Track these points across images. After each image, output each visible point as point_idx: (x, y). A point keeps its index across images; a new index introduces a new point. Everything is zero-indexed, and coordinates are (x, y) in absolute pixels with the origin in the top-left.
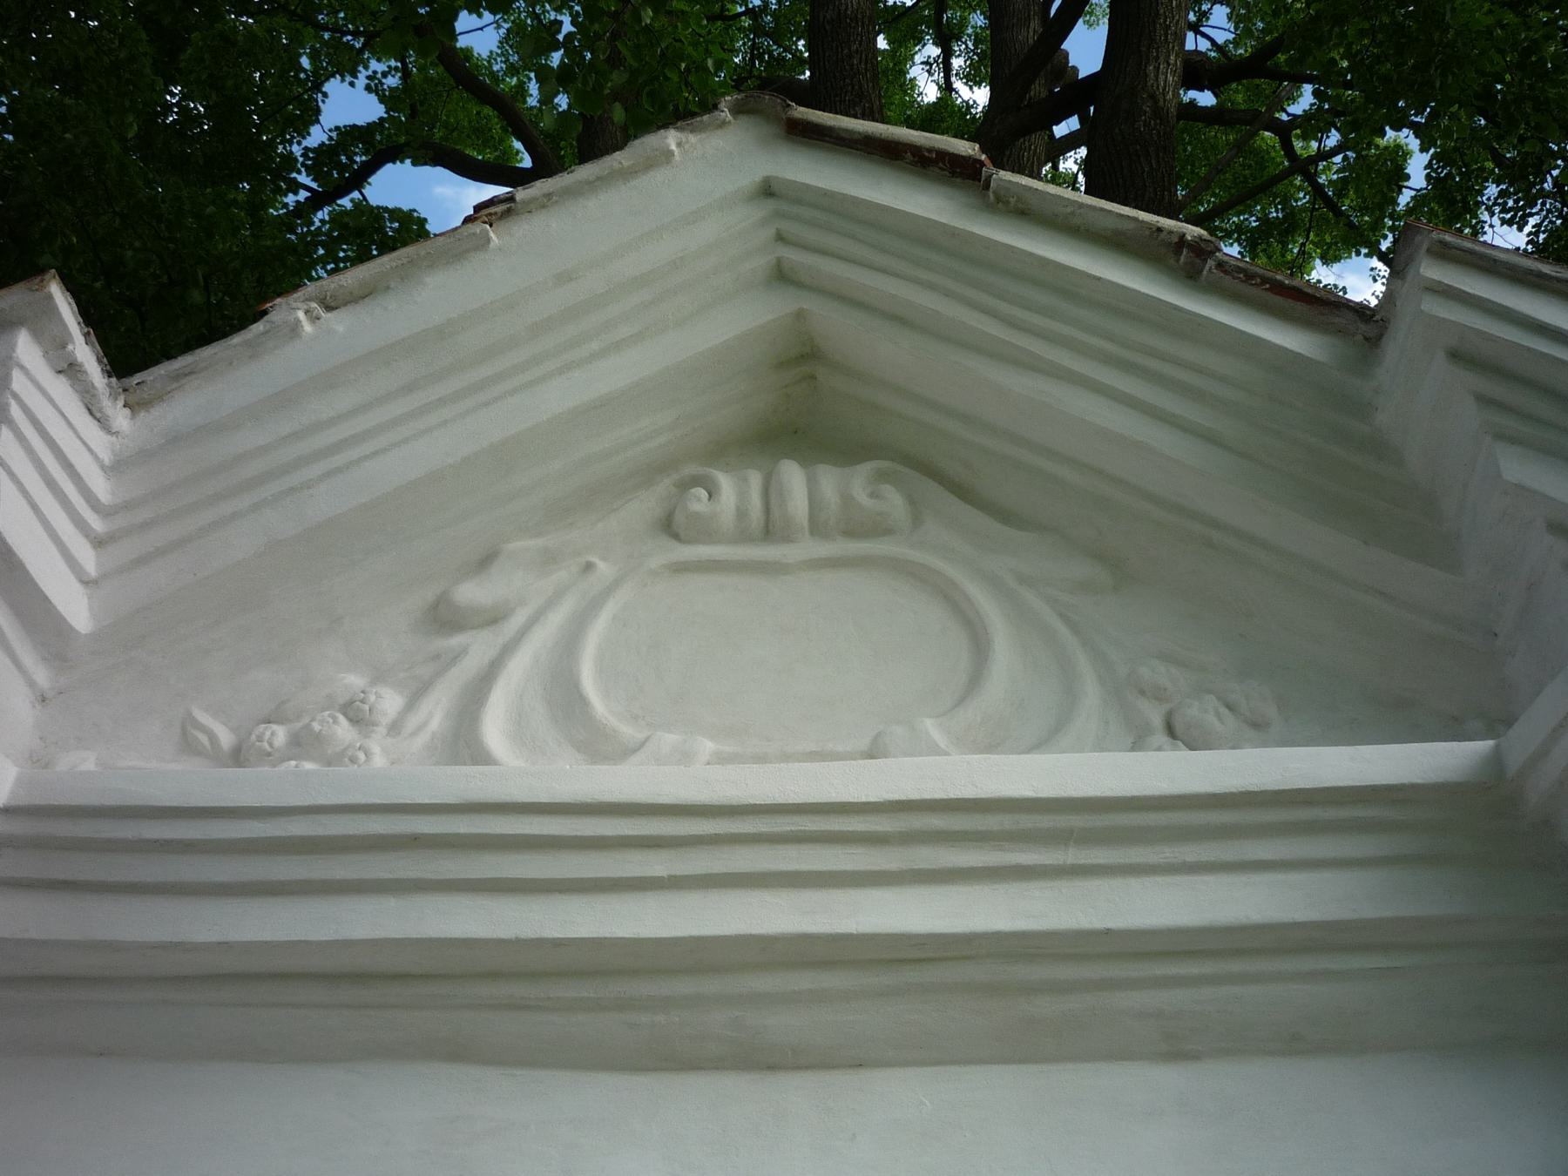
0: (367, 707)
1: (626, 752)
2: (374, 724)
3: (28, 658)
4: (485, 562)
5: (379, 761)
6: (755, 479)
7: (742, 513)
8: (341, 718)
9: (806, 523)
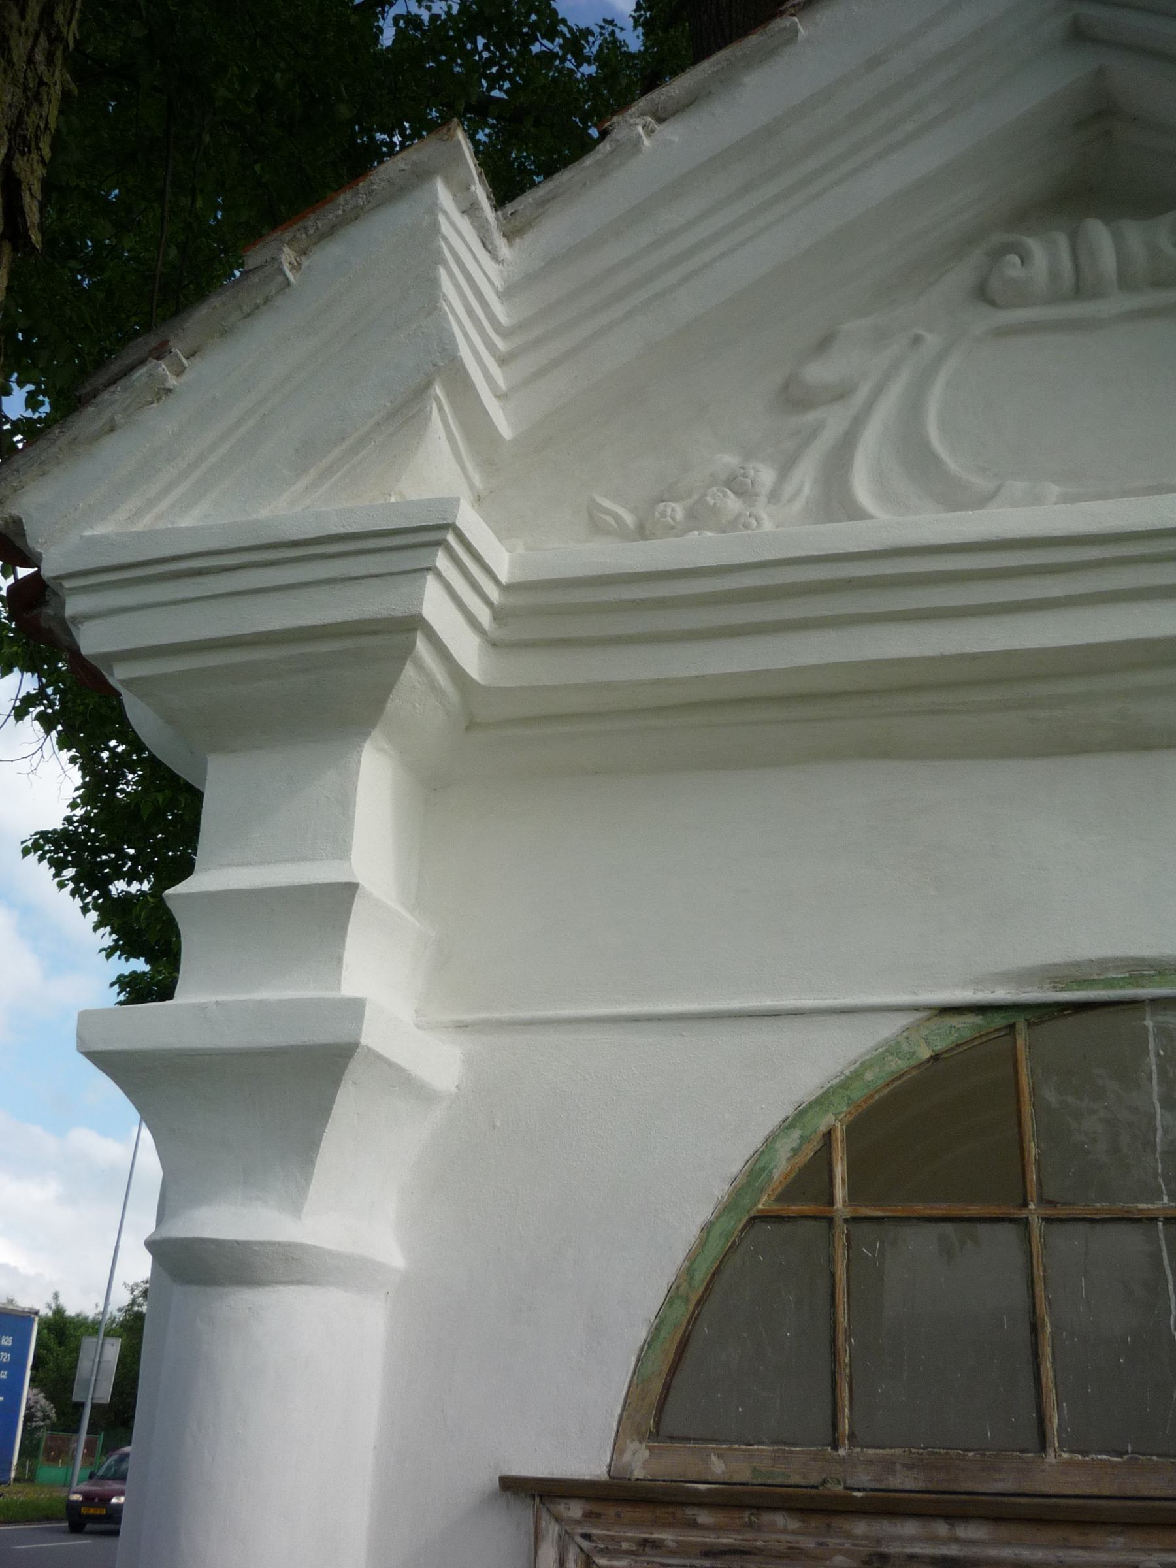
0: (749, 481)
1: (982, 501)
2: (757, 495)
4: (824, 344)
5: (768, 526)
6: (1062, 240)
7: (1054, 276)
9: (1114, 277)
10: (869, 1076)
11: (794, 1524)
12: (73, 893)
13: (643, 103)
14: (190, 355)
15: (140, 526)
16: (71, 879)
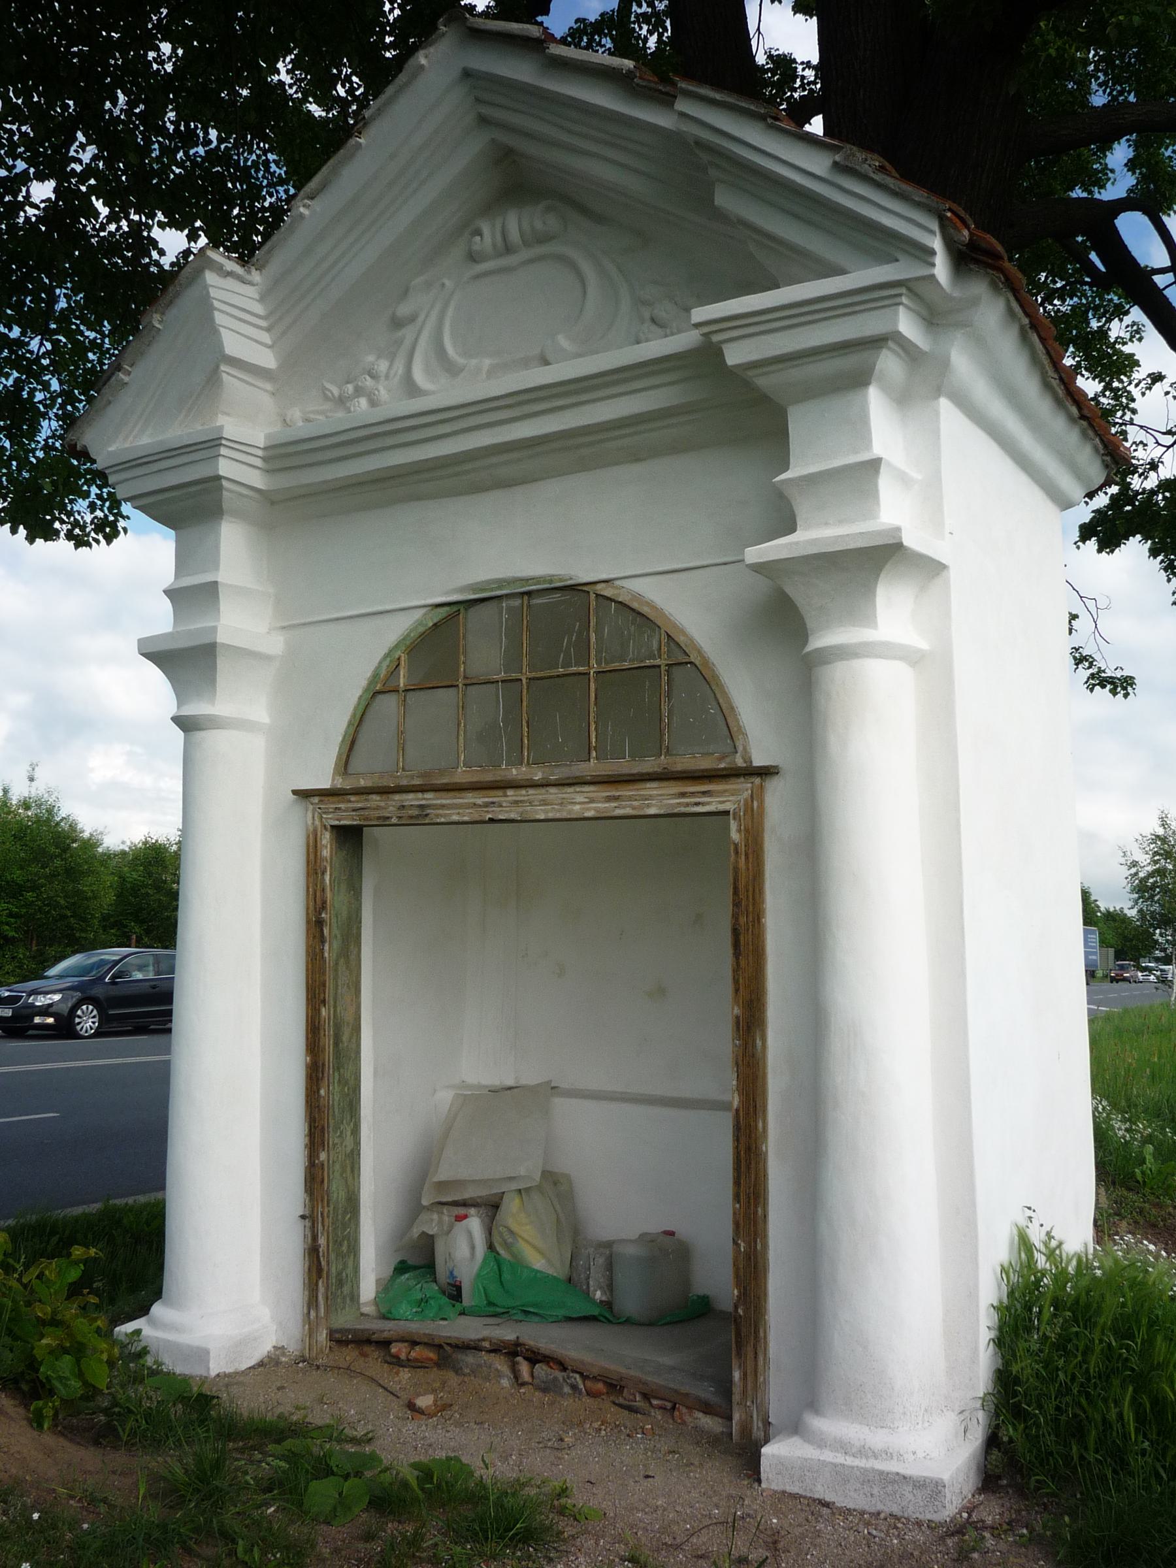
3: (260, 383)
4: (405, 293)
7: (494, 245)
8: (368, 378)
14: (132, 366)
15: (127, 445)
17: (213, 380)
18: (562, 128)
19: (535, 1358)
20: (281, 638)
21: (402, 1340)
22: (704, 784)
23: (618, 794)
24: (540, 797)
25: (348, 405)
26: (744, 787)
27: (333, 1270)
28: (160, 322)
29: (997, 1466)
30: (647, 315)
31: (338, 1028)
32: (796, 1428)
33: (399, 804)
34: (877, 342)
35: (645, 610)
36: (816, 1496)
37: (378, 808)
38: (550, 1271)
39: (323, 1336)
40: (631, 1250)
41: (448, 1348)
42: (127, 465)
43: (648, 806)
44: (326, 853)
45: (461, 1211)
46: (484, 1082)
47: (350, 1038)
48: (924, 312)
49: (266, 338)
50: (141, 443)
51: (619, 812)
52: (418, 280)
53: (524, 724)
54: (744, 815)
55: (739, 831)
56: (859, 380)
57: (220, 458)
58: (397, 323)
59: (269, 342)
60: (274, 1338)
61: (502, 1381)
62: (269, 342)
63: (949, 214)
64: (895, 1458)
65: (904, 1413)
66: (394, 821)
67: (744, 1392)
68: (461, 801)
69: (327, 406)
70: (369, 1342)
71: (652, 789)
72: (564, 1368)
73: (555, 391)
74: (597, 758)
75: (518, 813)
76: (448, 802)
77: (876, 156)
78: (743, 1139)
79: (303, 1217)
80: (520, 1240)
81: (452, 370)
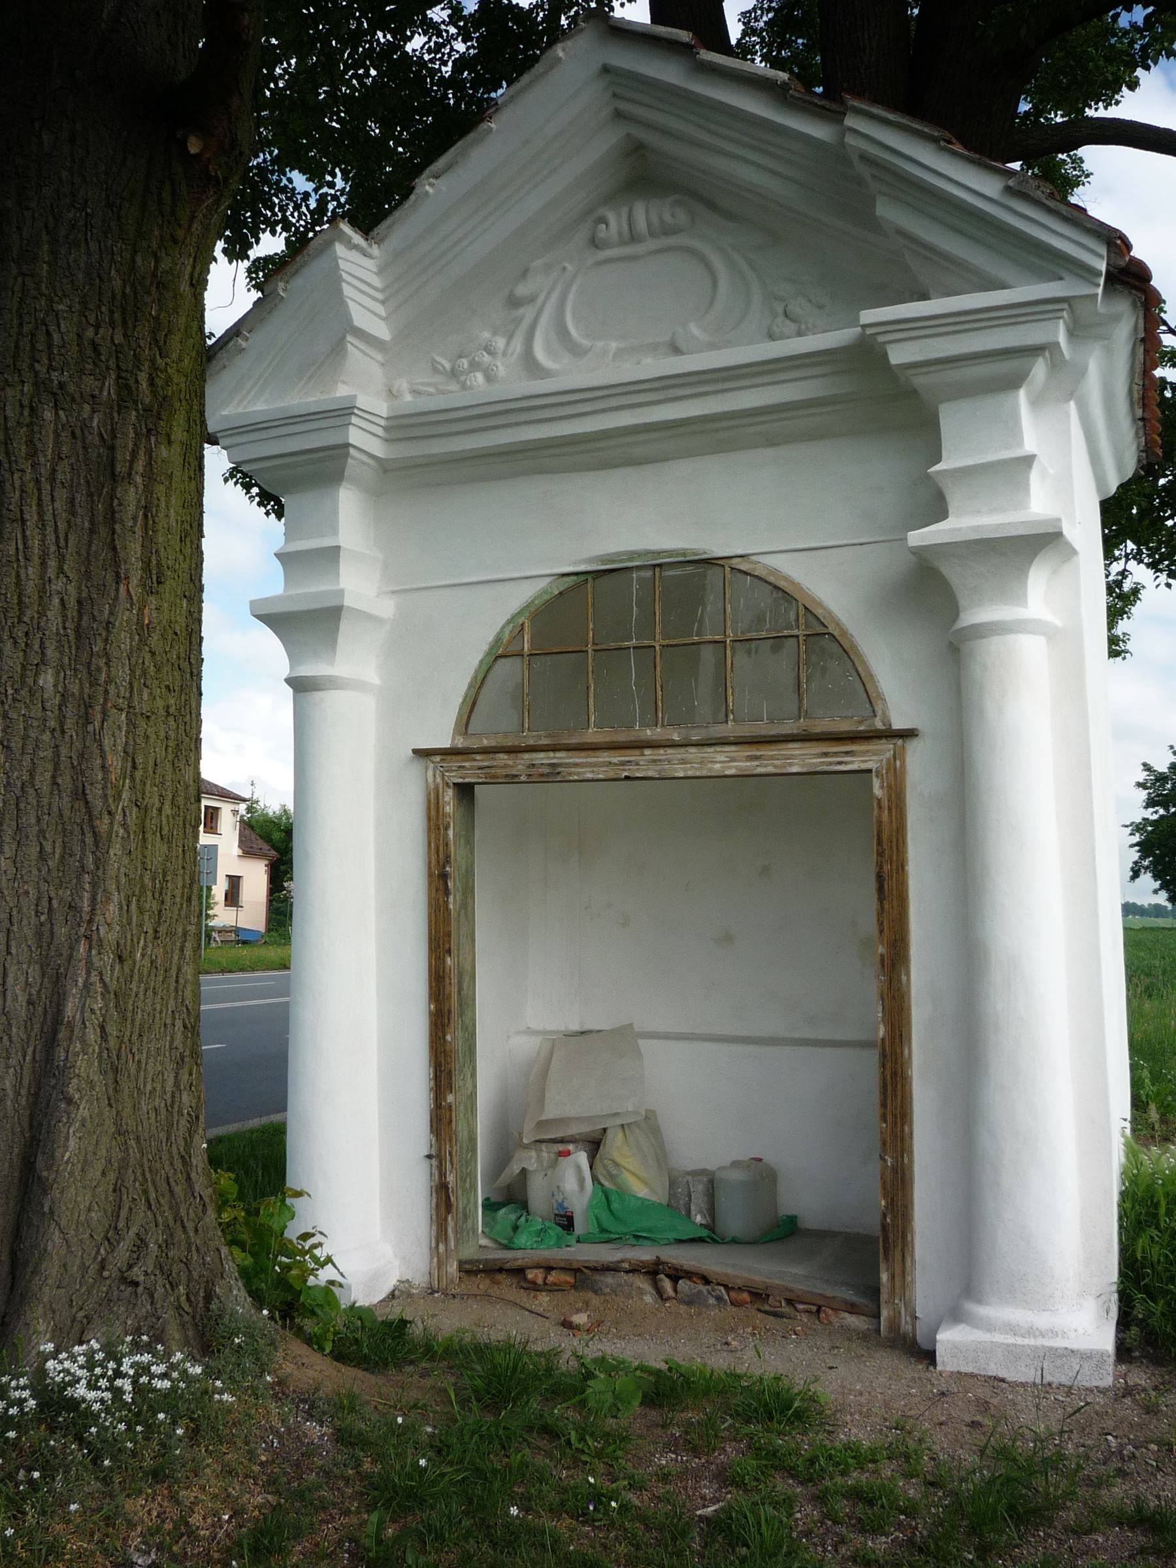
4: (525, 273)
7: (620, 234)
8: (485, 353)
10: (537, 602)
11: (506, 757)
12: (259, 504)
13: (427, 172)
15: (241, 410)
16: (257, 495)
17: (338, 350)
18: (701, 127)
19: (676, 1275)
20: (393, 603)
21: (538, 1267)
22: (847, 744)
23: (759, 753)
24: (679, 756)
25: (463, 378)
26: (886, 748)
27: (460, 1205)
28: (284, 290)
29: (1135, 1340)
30: (780, 309)
31: (460, 975)
32: (956, 1315)
33: (529, 762)
34: (1035, 351)
35: (782, 584)
36: (990, 1374)
37: (506, 766)
38: (654, 1199)
39: (453, 1268)
40: (735, 1175)
41: (586, 1271)
42: (240, 430)
43: (791, 765)
44: (449, 809)
45: (561, 1147)
46: (549, 1027)
47: (469, 987)
48: (1071, 325)
49: (381, 310)
50: (256, 408)
51: (760, 770)
52: (538, 263)
53: (659, 688)
54: (887, 773)
55: (882, 787)
56: (1013, 382)
57: (351, 427)
58: (514, 302)
59: (384, 314)
60: (398, 1273)
61: (645, 1298)
62: (384, 314)
63: (1119, 242)
64: (1060, 1335)
65: (1063, 1297)
66: (523, 778)
67: (892, 1292)
68: (595, 759)
69: (437, 379)
70: (500, 1270)
71: (794, 749)
72: (706, 1280)
73: (703, 377)
74: (734, 720)
75: (656, 771)
76: (581, 760)
77: (1048, 184)
78: (888, 1065)
79: (429, 1157)
80: (624, 1171)
81: (575, 350)
